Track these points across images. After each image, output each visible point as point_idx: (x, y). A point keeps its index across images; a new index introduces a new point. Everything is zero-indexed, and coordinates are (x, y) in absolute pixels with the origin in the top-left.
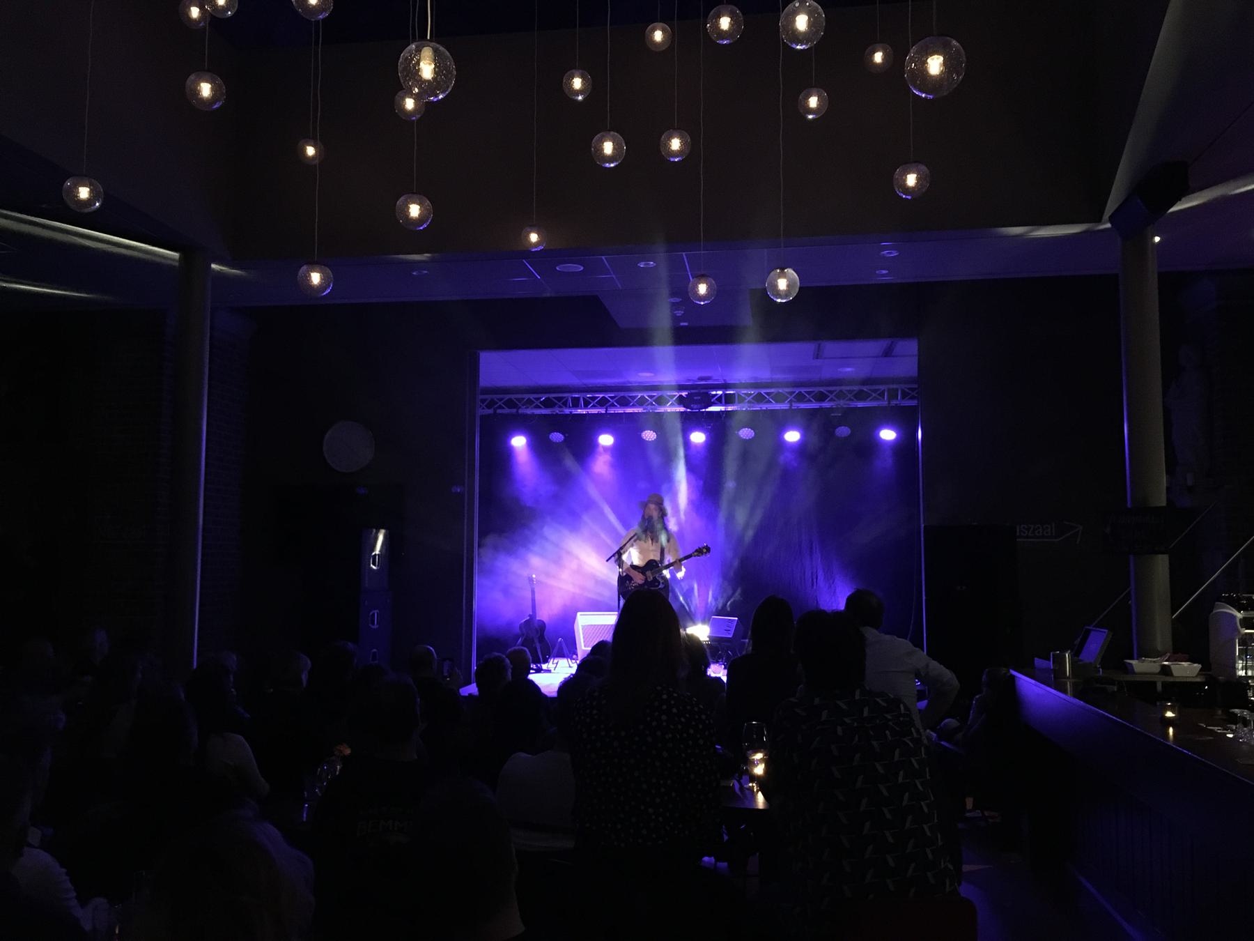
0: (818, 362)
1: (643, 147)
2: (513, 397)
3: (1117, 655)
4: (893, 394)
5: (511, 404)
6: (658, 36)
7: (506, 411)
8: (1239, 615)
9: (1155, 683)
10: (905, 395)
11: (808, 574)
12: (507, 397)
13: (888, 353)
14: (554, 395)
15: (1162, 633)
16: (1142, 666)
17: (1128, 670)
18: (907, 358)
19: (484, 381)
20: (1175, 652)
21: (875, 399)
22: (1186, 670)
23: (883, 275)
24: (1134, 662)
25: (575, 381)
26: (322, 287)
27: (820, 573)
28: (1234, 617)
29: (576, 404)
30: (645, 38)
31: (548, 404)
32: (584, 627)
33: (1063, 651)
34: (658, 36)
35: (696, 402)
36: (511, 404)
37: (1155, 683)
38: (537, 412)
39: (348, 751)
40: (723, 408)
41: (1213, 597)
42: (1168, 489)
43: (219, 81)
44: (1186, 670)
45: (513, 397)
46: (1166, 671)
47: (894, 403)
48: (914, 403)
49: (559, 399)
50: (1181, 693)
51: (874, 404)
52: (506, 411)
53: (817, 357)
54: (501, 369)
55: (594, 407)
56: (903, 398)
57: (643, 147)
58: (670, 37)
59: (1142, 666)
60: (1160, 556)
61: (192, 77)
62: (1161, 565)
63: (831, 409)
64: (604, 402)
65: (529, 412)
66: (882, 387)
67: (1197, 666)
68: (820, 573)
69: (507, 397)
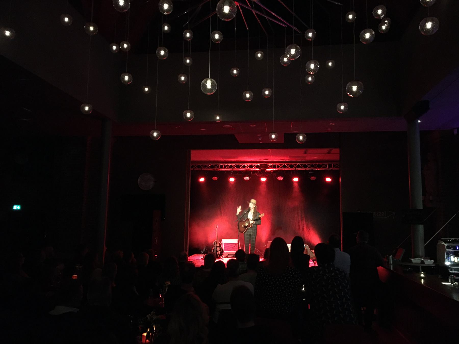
0: (305, 155)
1: (258, 94)
2: (200, 164)
3: (407, 257)
4: (330, 166)
5: (199, 167)
6: (259, 55)
7: (198, 169)
8: (446, 245)
9: (419, 266)
10: (334, 166)
11: (301, 227)
12: (198, 164)
13: (329, 153)
14: (216, 164)
15: (421, 250)
16: (415, 261)
17: (411, 262)
18: (335, 154)
19: (192, 160)
20: (426, 256)
21: (324, 167)
22: (429, 262)
23: (329, 130)
24: (412, 259)
25: (222, 159)
26: (157, 137)
27: (305, 227)
28: (444, 245)
29: (222, 167)
30: (255, 56)
31: (212, 167)
32: (224, 244)
33: (390, 255)
34: (259, 55)
35: (263, 167)
36: (199, 167)
37: (419, 266)
38: (208, 170)
39: (169, 283)
40: (272, 170)
41: (438, 239)
42: (423, 201)
43: (131, 76)
44: (429, 262)
45: (200, 164)
46: (423, 262)
47: (330, 169)
48: (338, 169)
49: (216, 165)
50: (426, 269)
51: (324, 169)
52: (198, 169)
53: (305, 153)
54: (197, 156)
55: (228, 168)
56: (334, 167)
57: (258, 94)
58: (263, 56)
59: (415, 261)
60: (421, 225)
61: (123, 74)
62: (421, 228)
63: (309, 171)
64: (231, 167)
65: (205, 169)
66: (326, 163)
67: (433, 261)
68: (305, 227)
69: (198, 164)
